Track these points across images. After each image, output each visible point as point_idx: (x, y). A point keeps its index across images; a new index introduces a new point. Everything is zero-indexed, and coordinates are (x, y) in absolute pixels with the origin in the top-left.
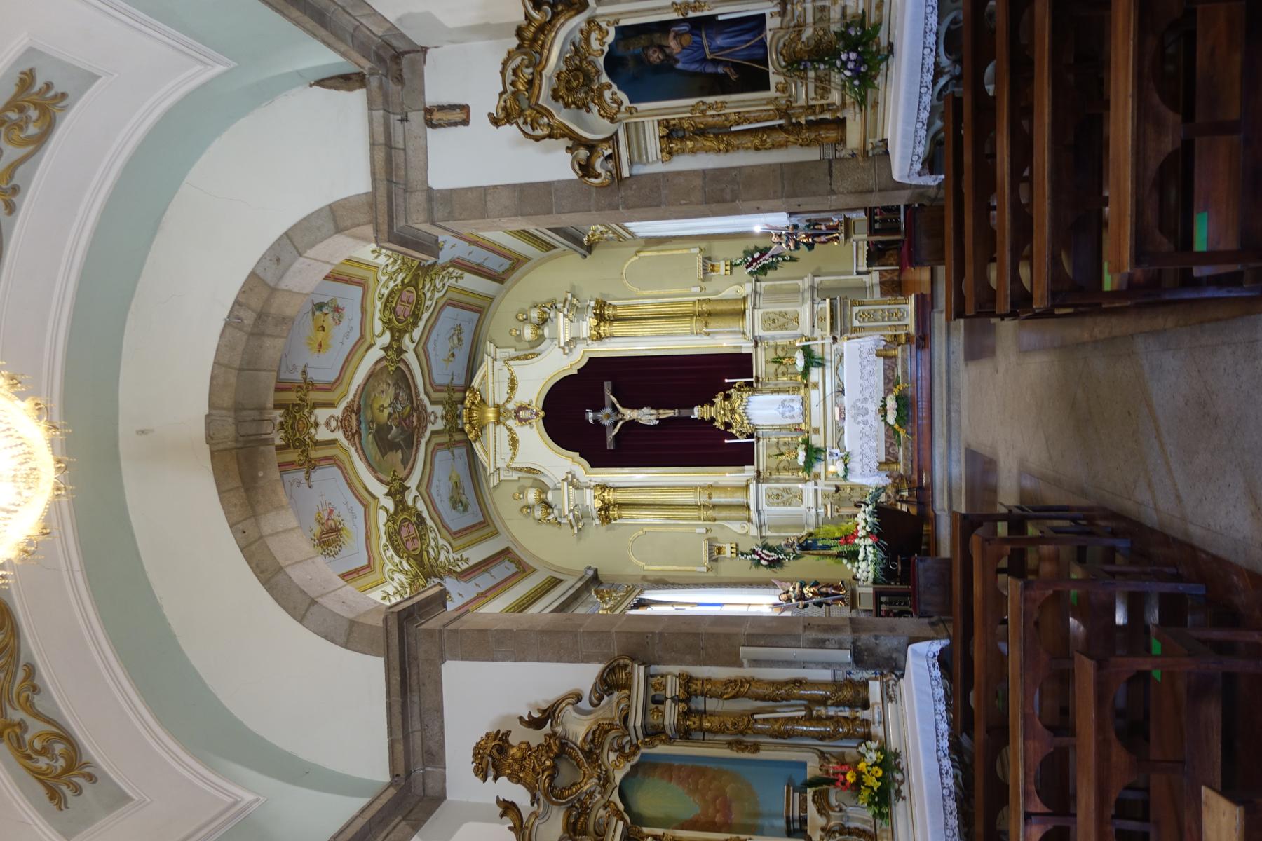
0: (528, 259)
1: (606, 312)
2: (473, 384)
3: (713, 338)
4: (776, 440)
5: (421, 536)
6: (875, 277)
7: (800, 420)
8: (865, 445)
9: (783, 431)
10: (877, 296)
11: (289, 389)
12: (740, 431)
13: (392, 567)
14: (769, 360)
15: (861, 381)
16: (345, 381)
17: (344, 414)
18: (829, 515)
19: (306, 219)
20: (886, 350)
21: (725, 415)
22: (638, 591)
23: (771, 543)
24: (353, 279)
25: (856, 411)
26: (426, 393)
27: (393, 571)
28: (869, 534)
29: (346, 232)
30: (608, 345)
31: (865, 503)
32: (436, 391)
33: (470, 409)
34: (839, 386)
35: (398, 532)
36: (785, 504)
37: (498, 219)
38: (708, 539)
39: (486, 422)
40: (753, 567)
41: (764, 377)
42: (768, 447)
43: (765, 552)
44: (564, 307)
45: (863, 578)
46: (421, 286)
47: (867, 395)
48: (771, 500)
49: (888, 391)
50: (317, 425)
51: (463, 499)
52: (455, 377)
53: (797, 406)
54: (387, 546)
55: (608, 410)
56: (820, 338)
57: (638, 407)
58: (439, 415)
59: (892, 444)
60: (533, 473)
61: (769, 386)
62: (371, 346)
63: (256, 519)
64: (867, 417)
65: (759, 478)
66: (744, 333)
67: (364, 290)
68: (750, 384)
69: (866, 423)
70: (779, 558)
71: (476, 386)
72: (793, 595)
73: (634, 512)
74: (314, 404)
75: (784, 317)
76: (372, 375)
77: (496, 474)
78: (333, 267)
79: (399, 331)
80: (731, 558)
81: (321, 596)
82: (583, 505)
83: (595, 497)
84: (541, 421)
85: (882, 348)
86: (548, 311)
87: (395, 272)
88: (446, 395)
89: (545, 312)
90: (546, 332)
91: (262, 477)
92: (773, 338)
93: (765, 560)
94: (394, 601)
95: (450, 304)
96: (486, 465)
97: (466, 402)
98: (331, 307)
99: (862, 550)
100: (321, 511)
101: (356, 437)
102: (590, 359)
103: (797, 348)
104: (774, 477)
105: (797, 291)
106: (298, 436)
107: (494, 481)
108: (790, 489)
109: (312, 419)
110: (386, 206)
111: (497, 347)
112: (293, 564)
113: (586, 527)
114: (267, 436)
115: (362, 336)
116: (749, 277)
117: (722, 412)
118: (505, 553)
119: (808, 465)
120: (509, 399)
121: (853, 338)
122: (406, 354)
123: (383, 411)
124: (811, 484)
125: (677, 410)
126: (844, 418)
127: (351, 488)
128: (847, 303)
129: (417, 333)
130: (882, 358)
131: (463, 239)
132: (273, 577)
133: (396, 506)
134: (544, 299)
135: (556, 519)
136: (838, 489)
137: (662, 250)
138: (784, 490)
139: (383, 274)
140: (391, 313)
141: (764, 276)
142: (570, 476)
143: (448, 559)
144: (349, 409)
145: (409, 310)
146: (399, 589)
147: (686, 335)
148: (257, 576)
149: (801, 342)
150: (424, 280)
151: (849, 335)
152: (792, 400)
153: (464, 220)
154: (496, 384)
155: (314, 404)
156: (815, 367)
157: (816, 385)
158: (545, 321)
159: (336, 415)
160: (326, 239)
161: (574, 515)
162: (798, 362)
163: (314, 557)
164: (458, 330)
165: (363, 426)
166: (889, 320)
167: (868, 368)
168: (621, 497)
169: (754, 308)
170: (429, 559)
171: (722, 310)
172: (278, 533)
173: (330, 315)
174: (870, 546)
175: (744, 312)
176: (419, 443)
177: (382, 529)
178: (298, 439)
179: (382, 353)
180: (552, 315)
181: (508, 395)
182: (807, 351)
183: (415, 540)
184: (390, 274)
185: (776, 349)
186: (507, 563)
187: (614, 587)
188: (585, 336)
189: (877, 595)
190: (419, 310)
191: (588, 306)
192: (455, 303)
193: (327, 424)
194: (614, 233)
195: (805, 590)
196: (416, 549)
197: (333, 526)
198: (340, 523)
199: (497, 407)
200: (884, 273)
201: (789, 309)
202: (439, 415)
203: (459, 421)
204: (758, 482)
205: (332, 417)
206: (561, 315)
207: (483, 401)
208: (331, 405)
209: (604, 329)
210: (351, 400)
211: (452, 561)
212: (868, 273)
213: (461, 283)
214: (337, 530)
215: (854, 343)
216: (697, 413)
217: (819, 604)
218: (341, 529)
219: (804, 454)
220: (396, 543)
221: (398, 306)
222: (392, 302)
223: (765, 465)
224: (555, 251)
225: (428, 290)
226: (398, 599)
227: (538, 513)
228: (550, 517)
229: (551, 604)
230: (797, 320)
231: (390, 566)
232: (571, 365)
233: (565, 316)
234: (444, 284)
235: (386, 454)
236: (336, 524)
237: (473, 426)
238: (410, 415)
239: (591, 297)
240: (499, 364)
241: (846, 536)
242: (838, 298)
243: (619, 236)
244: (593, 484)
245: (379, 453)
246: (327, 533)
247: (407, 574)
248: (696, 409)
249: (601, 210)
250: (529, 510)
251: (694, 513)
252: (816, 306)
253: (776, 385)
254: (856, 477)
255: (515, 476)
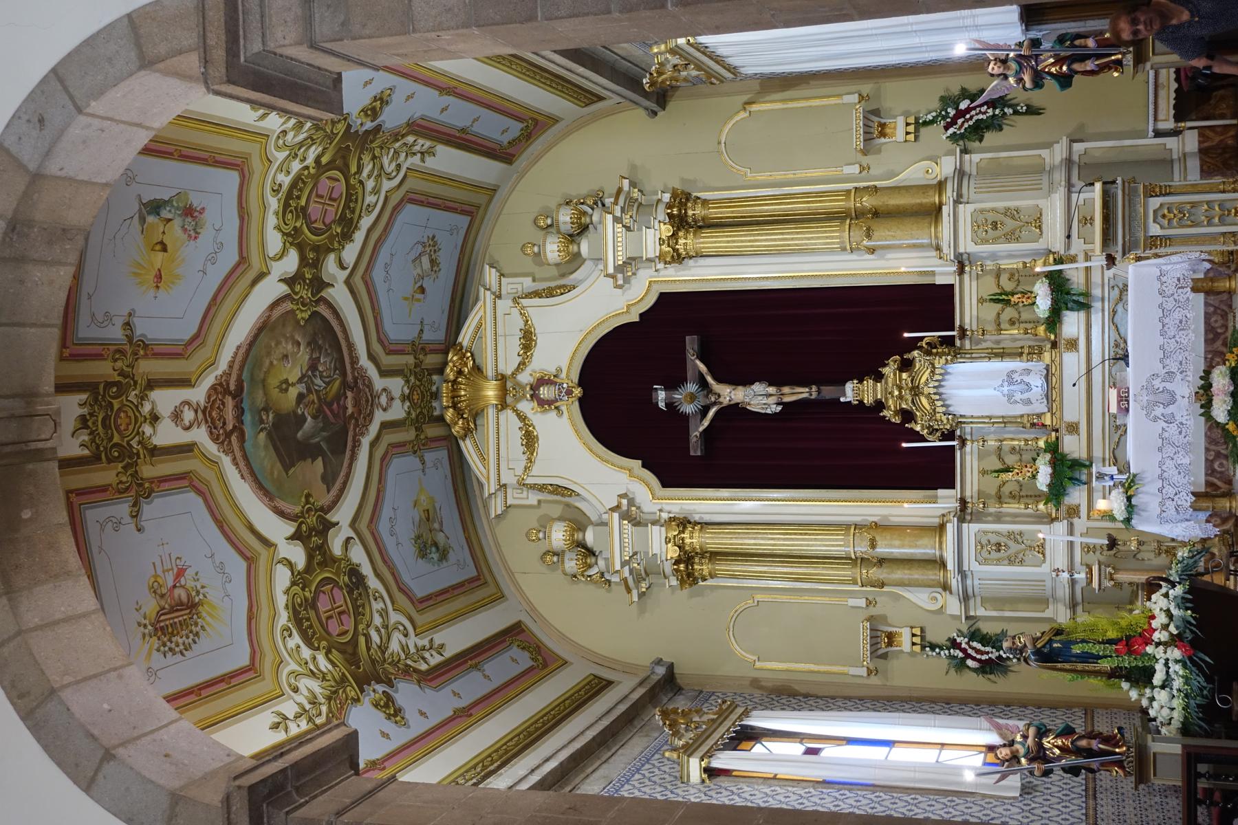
0: (555, 120)
1: (690, 212)
2: (460, 339)
3: (882, 258)
4: (998, 444)
5: (356, 607)
6: (1191, 141)
7: (1041, 407)
8: (1168, 462)
9: (1010, 428)
10: (1194, 176)
11: (98, 357)
12: (929, 427)
13: (297, 668)
14: (985, 297)
15: (1161, 341)
16: (212, 339)
17: (209, 397)
18: (1095, 584)
19: (90, 42)
20: (1212, 280)
21: (901, 397)
22: (740, 710)
23: (987, 628)
24: (218, 157)
25: (1151, 398)
26: (372, 357)
27: (297, 675)
28: (1175, 640)
29: (161, 66)
30: (693, 271)
31: (1166, 580)
32: (390, 352)
33: (454, 382)
34: (1117, 346)
35: (312, 604)
36: (1011, 561)
37: (433, 35)
38: (870, 619)
39: (482, 404)
40: (952, 671)
41: (974, 328)
42: (982, 455)
43: (975, 644)
44: (616, 203)
45: (1160, 719)
46: (353, 169)
47: (1174, 367)
48: (985, 554)
49: (1213, 358)
50: (155, 418)
51: (440, 538)
52: (426, 328)
53: (1037, 382)
54: (288, 629)
55: (691, 387)
56: (1081, 257)
57: (746, 381)
58: (397, 393)
59: (1218, 455)
60: (563, 495)
61: (984, 345)
62: (261, 276)
63: (9, 600)
64: (1171, 409)
65: (964, 511)
66: (938, 248)
67: (243, 176)
68: (949, 341)
69: (1170, 420)
70: (1000, 657)
71: (465, 344)
72: (1022, 751)
73: (738, 567)
74: (149, 380)
75: (1013, 217)
76: (264, 328)
77: (500, 495)
78: (151, 134)
79: (316, 248)
80: (912, 654)
81: (123, 744)
82: (646, 553)
83: (667, 541)
84: (577, 404)
85: (1202, 276)
86: (590, 211)
87: (301, 144)
88: (410, 360)
89: (585, 213)
90: (584, 247)
91: (30, 519)
92: (994, 256)
93: (974, 659)
94: (294, 730)
95: (412, 201)
96: (484, 481)
97: (448, 370)
98: (178, 208)
99: (1159, 667)
100: (159, 572)
101: (234, 438)
102: (662, 295)
103: (1038, 274)
104: (992, 510)
105: (1039, 170)
106: (116, 439)
107: (496, 507)
108: (1021, 534)
109: (147, 408)
110: (222, 13)
111: (502, 275)
112: (78, 682)
113: (655, 589)
114: (40, 445)
115: (243, 259)
116: (949, 145)
117: (896, 393)
118: (514, 633)
119: (1057, 492)
120: (522, 366)
121: (1148, 258)
122: (330, 290)
123: (286, 390)
124: (1061, 527)
125: (814, 388)
126: (1127, 410)
127: (221, 528)
128: (1136, 190)
129: (350, 253)
130: (1202, 296)
131: (427, 83)
132: (38, 706)
133: (310, 558)
134: (584, 191)
135: (602, 575)
136: (1113, 543)
137: (792, 100)
138: (1010, 535)
139: (278, 148)
140: (298, 217)
141: (977, 144)
142: (624, 502)
143: (404, 648)
144: (219, 389)
145: (333, 212)
146: (308, 707)
147: (832, 251)
148: (13, 704)
149: (1045, 264)
150: (360, 159)
151: (1140, 253)
152: (1028, 371)
153: (370, 37)
154: (501, 340)
155: (149, 380)
156: (1072, 309)
157: (1072, 344)
158: (583, 229)
159: (194, 400)
160: (123, 79)
161: (631, 571)
162: (1039, 301)
163: (122, 667)
164: (431, 245)
165: (247, 418)
166: (1222, 222)
167: (1177, 315)
168: (713, 541)
169: (957, 202)
170: (368, 649)
171: (898, 206)
172: (56, 623)
173: (177, 222)
174: (1177, 661)
175: (938, 209)
176: (356, 444)
177: (281, 600)
178: (116, 445)
179: (284, 289)
180: (595, 218)
181: (520, 359)
182: (1057, 282)
183: (343, 617)
184: (291, 148)
185: (998, 276)
186: (515, 651)
187: (701, 695)
188: (651, 255)
189: (1191, 759)
190: (353, 212)
191: (659, 201)
192: (422, 198)
193: (177, 416)
194: (698, 68)
195: (1047, 742)
196: (345, 633)
197: (184, 598)
198: (198, 593)
199: (502, 379)
200: (1208, 133)
201: (1024, 202)
202: (397, 393)
203: (434, 404)
204: (962, 520)
205: (187, 403)
206: (609, 217)
207: (478, 369)
208: (184, 382)
209: (686, 242)
210: (224, 373)
211: (413, 650)
212: (1175, 133)
213: (430, 162)
214: (192, 606)
215: (1150, 268)
216: (850, 392)
217: (1074, 771)
218: (200, 603)
219: (1049, 470)
220: (306, 624)
221: (312, 206)
222: (299, 198)
223: (976, 488)
224: (600, 105)
225: (369, 176)
226: (304, 725)
227: (571, 564)
228: (591, 572)
229: (582, 733)
230: (976, 226)
231: (293, 666)
232: (628, 306)
233: (617, 220)
234: (399, 166)
235: (293, 465)
236: (189, 596)
237: (459, 413)
238: (340, 396)
239: (665, 186)
240: (504, 305)
241: (1129, 638)
242: (1119, 181)
243: (710, 74)
244: (665, 516)
245: (279, 464)
246: (172, 611)
247: (324, 679)
248: (849, 387)
249: (631, 10)
250: (555, 559)
251: (846, 572)
252: (1074, 196)
253: (998, 342)
254: (1147, 521)
255: (533, 498)
